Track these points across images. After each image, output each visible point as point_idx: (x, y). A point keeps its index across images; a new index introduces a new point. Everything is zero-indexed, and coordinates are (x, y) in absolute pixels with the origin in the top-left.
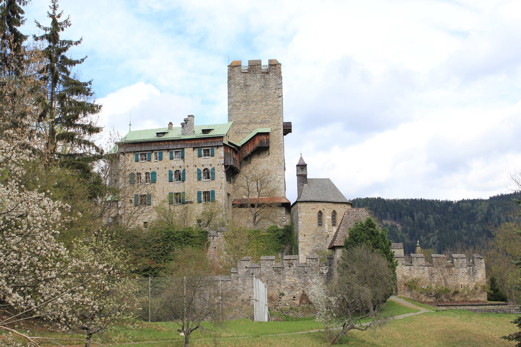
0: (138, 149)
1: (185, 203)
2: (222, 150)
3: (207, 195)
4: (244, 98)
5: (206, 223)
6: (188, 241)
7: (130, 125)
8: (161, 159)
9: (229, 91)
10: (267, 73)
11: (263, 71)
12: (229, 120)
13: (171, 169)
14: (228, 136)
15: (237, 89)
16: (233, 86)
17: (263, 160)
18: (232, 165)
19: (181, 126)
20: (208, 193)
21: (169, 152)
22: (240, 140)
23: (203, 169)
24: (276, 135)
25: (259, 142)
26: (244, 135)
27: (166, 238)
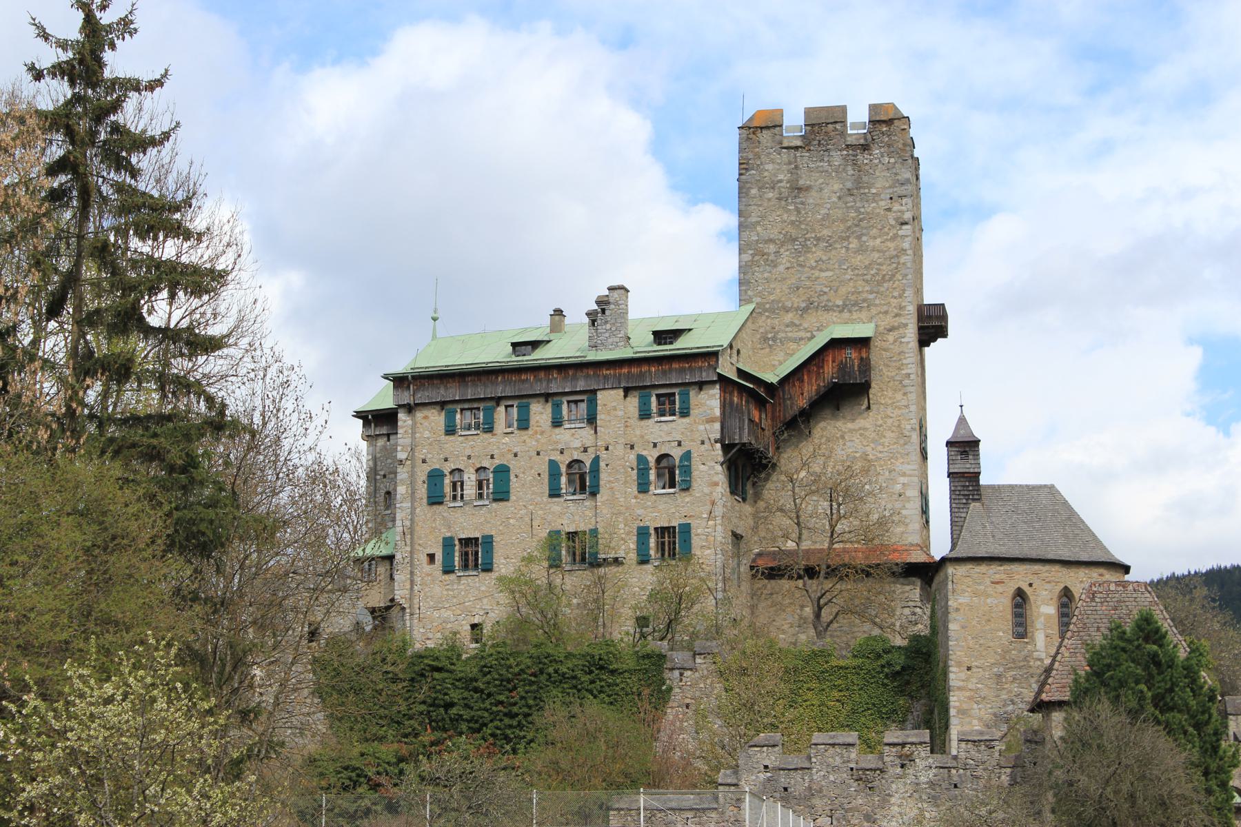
0: (454, 395)
1: (599, 565)
2: (714, 395)
3: (667, 539)
4: (789, 229)
5: (661, 626)
6: (603, 683)
7: (435, 319)
8: (524, 424)
9: (743, 208)
10: (865, 148)
11: (850, 141)
12: (743, 301)
13: (556, 457)
14: (735, 351)
15: (769, 200)
16: (754, 191)
17: (850, 425)
18: (744, 444)
19: (586, 320)
20: (669, 533)
21: (550, 404)
22: (777, 363)
23: (656, 454)
24: (892, 347)
25: (835, 370)
26: (789, 348)
27: (534, 675)
